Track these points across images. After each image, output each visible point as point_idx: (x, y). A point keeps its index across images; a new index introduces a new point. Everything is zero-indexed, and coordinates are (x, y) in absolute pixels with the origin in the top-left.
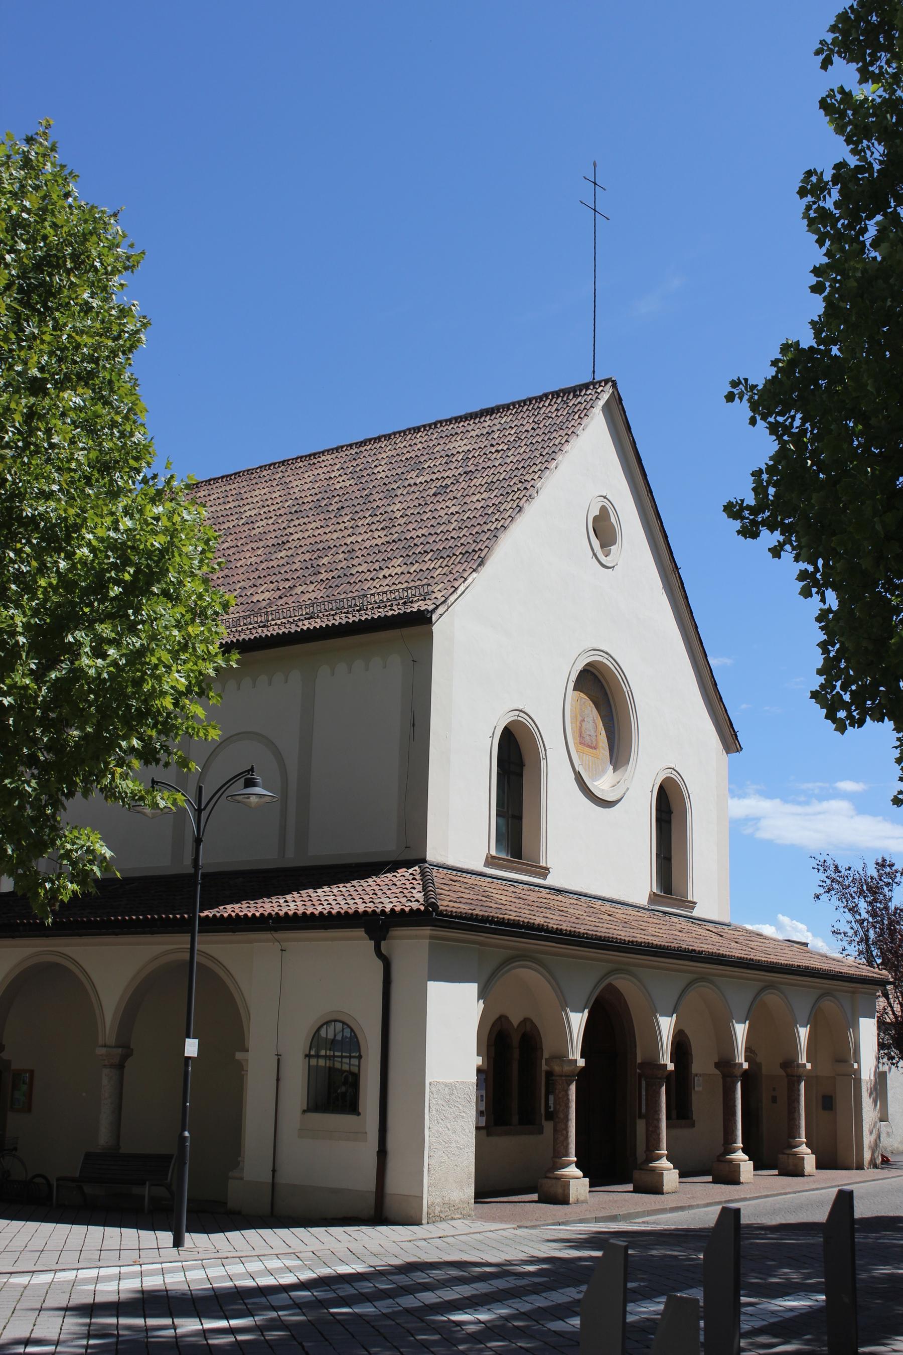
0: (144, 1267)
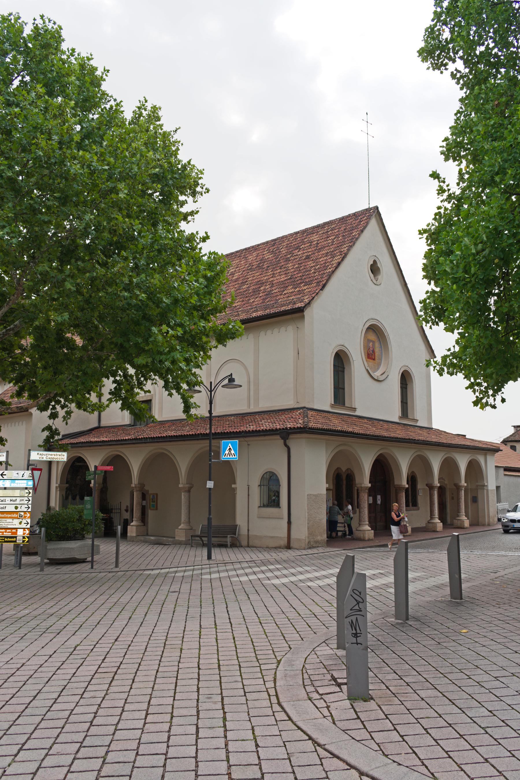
0: (195, 567)
